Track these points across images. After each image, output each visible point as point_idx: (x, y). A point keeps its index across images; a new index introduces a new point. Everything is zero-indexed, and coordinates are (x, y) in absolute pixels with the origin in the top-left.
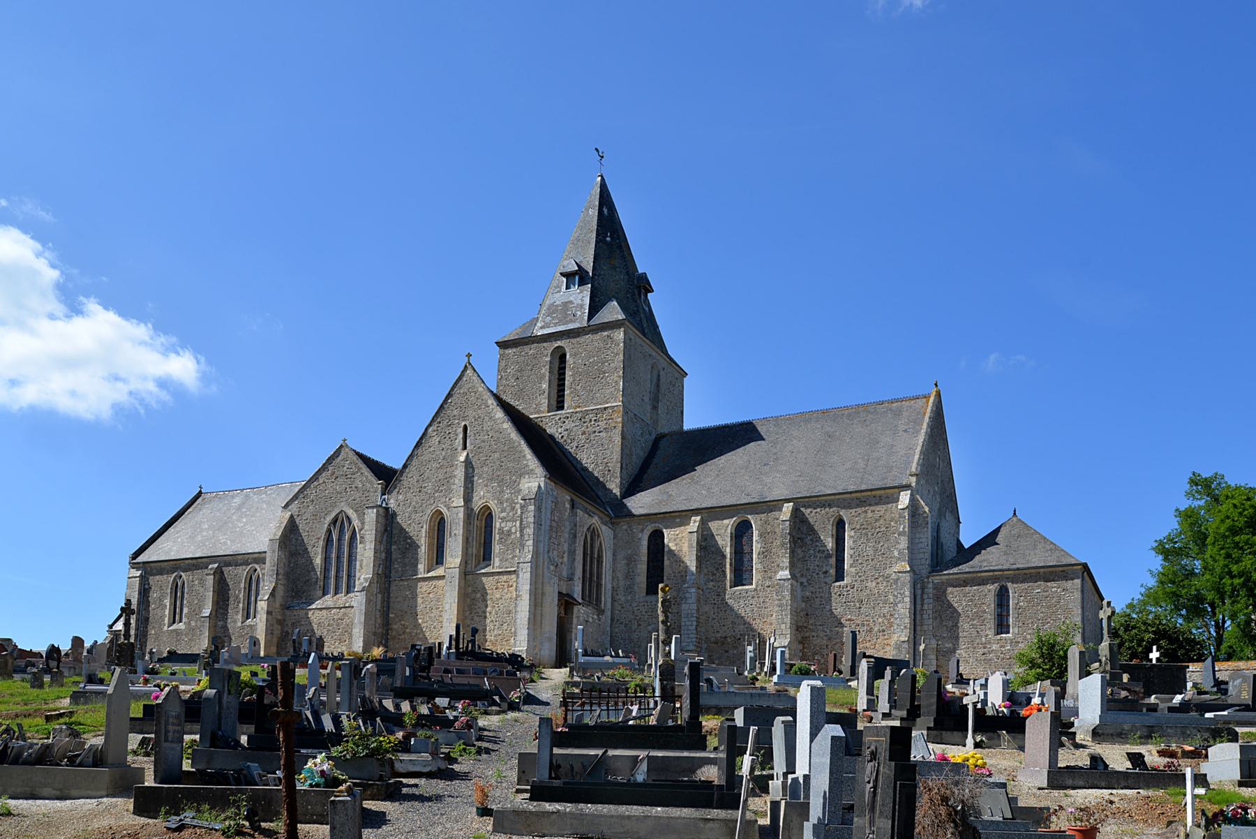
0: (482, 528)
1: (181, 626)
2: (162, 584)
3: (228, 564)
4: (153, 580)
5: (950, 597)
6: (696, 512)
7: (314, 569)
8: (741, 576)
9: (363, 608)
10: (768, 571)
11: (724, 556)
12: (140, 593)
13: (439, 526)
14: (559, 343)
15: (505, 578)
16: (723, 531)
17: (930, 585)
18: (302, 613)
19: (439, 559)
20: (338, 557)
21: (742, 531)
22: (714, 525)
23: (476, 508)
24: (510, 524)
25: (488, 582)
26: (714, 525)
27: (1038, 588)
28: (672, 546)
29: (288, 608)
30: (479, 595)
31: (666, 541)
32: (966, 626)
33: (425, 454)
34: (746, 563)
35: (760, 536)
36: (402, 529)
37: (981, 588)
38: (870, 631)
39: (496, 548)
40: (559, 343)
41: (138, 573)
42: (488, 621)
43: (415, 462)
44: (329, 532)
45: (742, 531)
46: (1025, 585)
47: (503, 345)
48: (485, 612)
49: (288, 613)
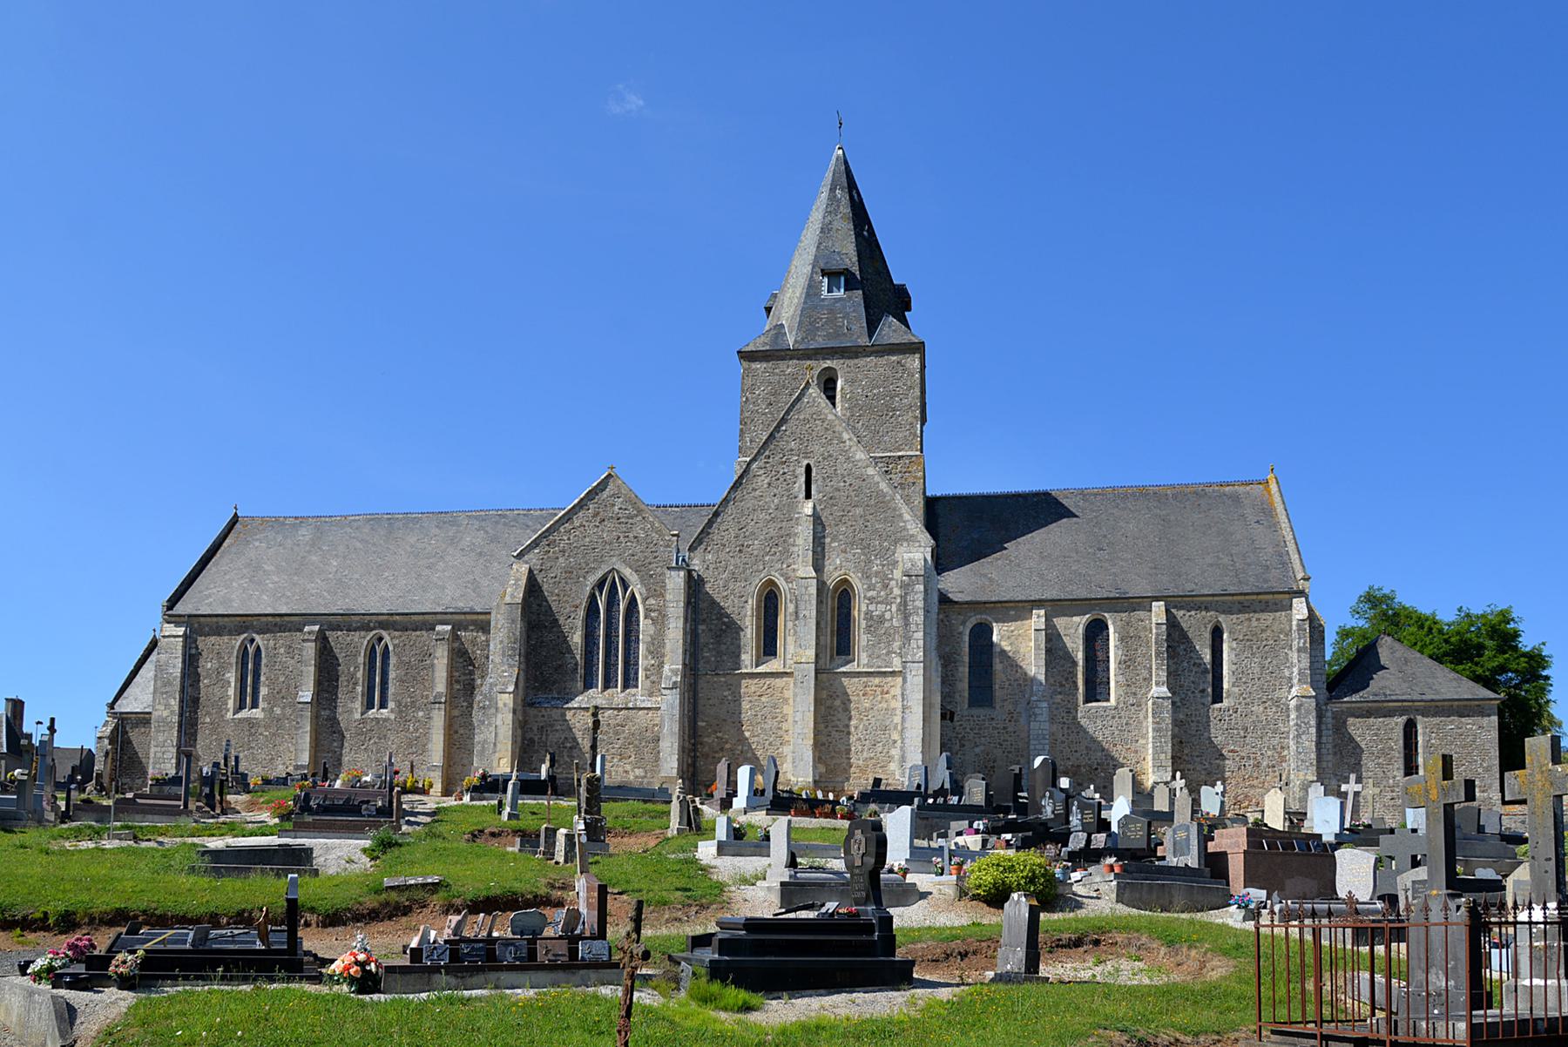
0: (838, 611)
1: (257, 713)
2: (221, 654)
3: (338, 628)
4: (205, 643)
5: (1351, 730)
6: (1038, 603)
7: (570, 651)
8: (1097, 688)
9: (676, 712)
10: (1134, 686)
11: (1075, 664)
12: (184, 662)
13: (770, 602)
14: (828, 363)
15: (877, 680)
16: (1073, 629)
17: (1329, 714)
18: (555, 713)
19: (769, 647)
20: (608, 636)
21: (1096, 632)
22: (1060, 622)
23: (831, 583)
24: (881, 607)
25: (851, 685)
26: (1060, 622)
27: (1452, 724)
28: (1006, 646)
29: (532, 705)
30: (838, 703)
31: (995, 638)
32: (1371, 765)
33: (747, 499)
34: (1101, 674)
35: (1122, 639)
36: (713, 602)
37: (1387, 720)
38: (1258, 765)
39: (861, 638)
40: (828, 363)
41: (181, 631)
42: (853, 739)
43: (731, 508)
44: (592, 600)
45: (1096, 632)
46: (1437, 720)
47: (747, 356)
48: (848, 726)
49: (532, 712)
